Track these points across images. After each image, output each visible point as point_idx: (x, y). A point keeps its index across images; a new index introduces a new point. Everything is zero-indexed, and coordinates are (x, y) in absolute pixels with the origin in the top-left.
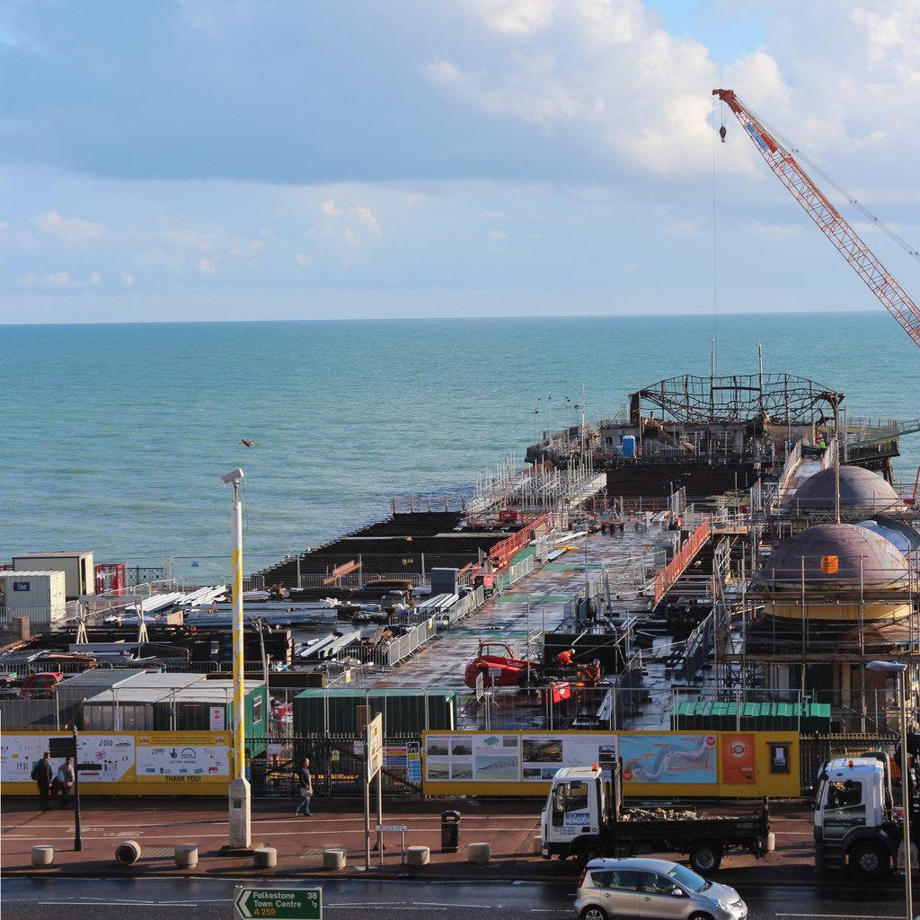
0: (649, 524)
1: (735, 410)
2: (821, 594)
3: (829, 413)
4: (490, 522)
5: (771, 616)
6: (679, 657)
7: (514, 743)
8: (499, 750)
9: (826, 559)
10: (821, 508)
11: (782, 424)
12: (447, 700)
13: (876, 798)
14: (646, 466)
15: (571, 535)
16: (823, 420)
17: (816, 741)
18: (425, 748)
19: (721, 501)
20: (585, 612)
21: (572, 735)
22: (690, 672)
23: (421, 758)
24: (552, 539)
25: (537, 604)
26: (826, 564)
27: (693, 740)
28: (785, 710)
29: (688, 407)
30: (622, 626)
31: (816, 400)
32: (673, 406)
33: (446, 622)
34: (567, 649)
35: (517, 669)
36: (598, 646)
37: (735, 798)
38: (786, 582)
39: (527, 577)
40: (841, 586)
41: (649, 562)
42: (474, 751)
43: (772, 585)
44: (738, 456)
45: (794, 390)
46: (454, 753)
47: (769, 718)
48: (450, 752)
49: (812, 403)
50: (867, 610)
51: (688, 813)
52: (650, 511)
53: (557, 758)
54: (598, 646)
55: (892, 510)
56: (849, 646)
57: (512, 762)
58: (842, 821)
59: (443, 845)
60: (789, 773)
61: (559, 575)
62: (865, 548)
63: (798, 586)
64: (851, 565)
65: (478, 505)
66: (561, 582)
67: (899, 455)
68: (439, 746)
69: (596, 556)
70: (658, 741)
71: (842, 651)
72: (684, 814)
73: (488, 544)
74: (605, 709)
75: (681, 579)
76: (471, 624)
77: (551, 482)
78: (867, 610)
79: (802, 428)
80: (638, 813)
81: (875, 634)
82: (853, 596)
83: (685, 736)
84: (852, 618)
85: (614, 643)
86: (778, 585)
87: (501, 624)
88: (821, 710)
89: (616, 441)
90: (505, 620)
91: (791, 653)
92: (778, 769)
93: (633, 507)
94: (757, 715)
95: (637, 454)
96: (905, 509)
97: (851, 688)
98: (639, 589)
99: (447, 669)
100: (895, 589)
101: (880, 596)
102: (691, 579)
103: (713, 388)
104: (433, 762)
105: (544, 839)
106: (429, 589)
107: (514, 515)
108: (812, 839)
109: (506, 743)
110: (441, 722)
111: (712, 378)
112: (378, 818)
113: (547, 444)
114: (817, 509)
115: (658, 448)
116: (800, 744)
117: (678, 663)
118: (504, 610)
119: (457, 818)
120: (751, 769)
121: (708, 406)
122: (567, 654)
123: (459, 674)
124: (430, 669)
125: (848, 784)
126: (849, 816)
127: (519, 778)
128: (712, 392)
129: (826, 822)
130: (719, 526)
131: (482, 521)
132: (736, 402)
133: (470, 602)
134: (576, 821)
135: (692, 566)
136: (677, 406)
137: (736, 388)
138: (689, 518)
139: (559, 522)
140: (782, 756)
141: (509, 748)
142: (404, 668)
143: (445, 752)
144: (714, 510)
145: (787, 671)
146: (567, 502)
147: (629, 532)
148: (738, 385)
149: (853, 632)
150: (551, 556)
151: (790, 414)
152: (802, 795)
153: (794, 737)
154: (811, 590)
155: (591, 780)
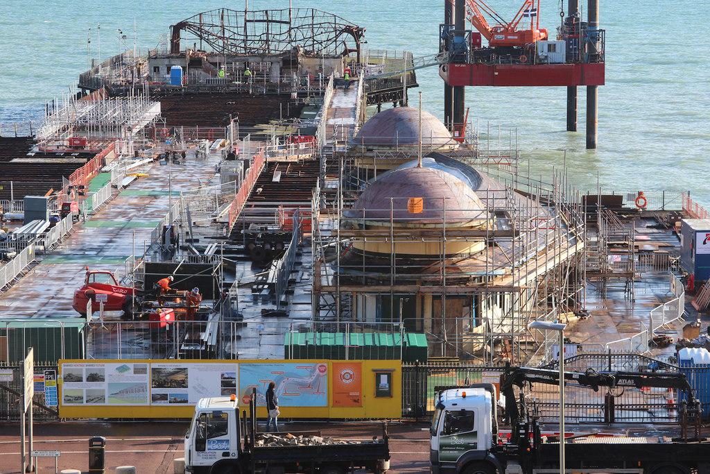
0: (208, 152)
1: (267, 41)
2: (408, 232)
3: (351, 45)
4: (61, 148)
5: (361, 251)
6: (264, 283)
7: (143, 371)
8: (130, 377)
9: (413, 201)
10: (383, 146)
11: (314, 57)
12: (79, 330)
13: (484, 425)
14: (191, 94)
15: (138, 162)
16: (346, 52)
17: (417, 369)
18: (61, 376)
19: (271, 129)
20: (168, 239)
21: (196, 364)
22: (276, 300)
23: (58, 385)
24: (123, 167)
25: (121, 230)
26: (413, 205)
27: (306, 368)
28: (386, 340)
29: (223, 38)
30: (205, 253)
31: (340, 34)
32: (211, 37)
33: (42, 248)
34: (166, 277)
35: (121, 295)
36: (192, 275)
37: (343, 420)
38: (375, 221)
39: (106, 203)
40: (425, 224)
41: (216, 189)
42: (107, 378)
43: (362, 223)
44: (275, 85)
45: (320, 24)
46: (88, 380)
47: (374, 347)
48: (84, 379)
49: (337, 36)
50: (450, 246)
51: (316, 438)
52: (206, 139)
53: (183, 384)
54: (192, 275)
55: (446, 147)
56: (431, 278)
57: (141, 388)
58: (456, 446)
59: (90, 467)
60: (392, 397)
61: (135, 201)
62: (445, 190)
63: (386, 224)
64: (433, 206)
65: (47, 132)
66: (139, 208)
67: (418, 86)
68: (75, 373)
69: (169, 183)
70: (275, 369)
71: (424, 283)
72: (313, 440)
73: (67, 170)
74: (210, 334)
75: (247, 206)
76: (65, 248)
77: (113, 111)
78: (450, 246)
79: (332, 61)
80: (271, 439)
81: (454, 267)
82: (439, 234)
83: (298, 365)
84: (433, 253)
85: (212, 271)
86: (368, 223)
87: (92, 249)
88: (418, 340)
89: (163, 71)
90: (96, 245)
91: (378, 284)
92: (381, 394)
93: (190, 135)
94: (363, 345)
95: (184, 83)
96: (457, 146)
97: (433, 316)
98: (213, 216)
99: (52, 293)
100: (472, 227)
101: (460, 234)
102: (256, 206)
103: (246, 21)
104: (68, 388)
105: (187, 463)
106: (21, 214)
107: (83, 142)
108: (428, 458)
109: (137, 371)
110: (75, 353)
111: (246, 12)
112: (22, 442)
113: (97, 71)
114: (380, 146)
115: (202, 76)
116: (403, 371)
117: (263, 289)
118: (91, 235)
119: (103, 443)
120: (358, 394)
121: (242, 38)
122: (166, 281)
123: (64, 298)
124: (36, 293)
125: (463, 412)
126: (462, 441)
127: (148, 402)
128: (245, 24)
129: (442, 446)
130: (273, 154)
131: (52, 147)
132: (268, 34)
133: (63, 226)
134: (216, 447)
135: (254, 193)
136: (215, 37)
137: (268, 21)
138: (245, 147)
139: (127, 149)
140: (386, 382)
141: (139, 375)
142: (12, 292)
143: (80, 380)
144: (264, 139)
145: (374, 300)
146: (130, 129)
147: (190, 162)
148: (270, 19)
149: (433, 267)
150: (126, 182)
151: (316, 46)
152: (403, 416)
153: (396, 365)
154: (399, 228)
155: (230, 410)
